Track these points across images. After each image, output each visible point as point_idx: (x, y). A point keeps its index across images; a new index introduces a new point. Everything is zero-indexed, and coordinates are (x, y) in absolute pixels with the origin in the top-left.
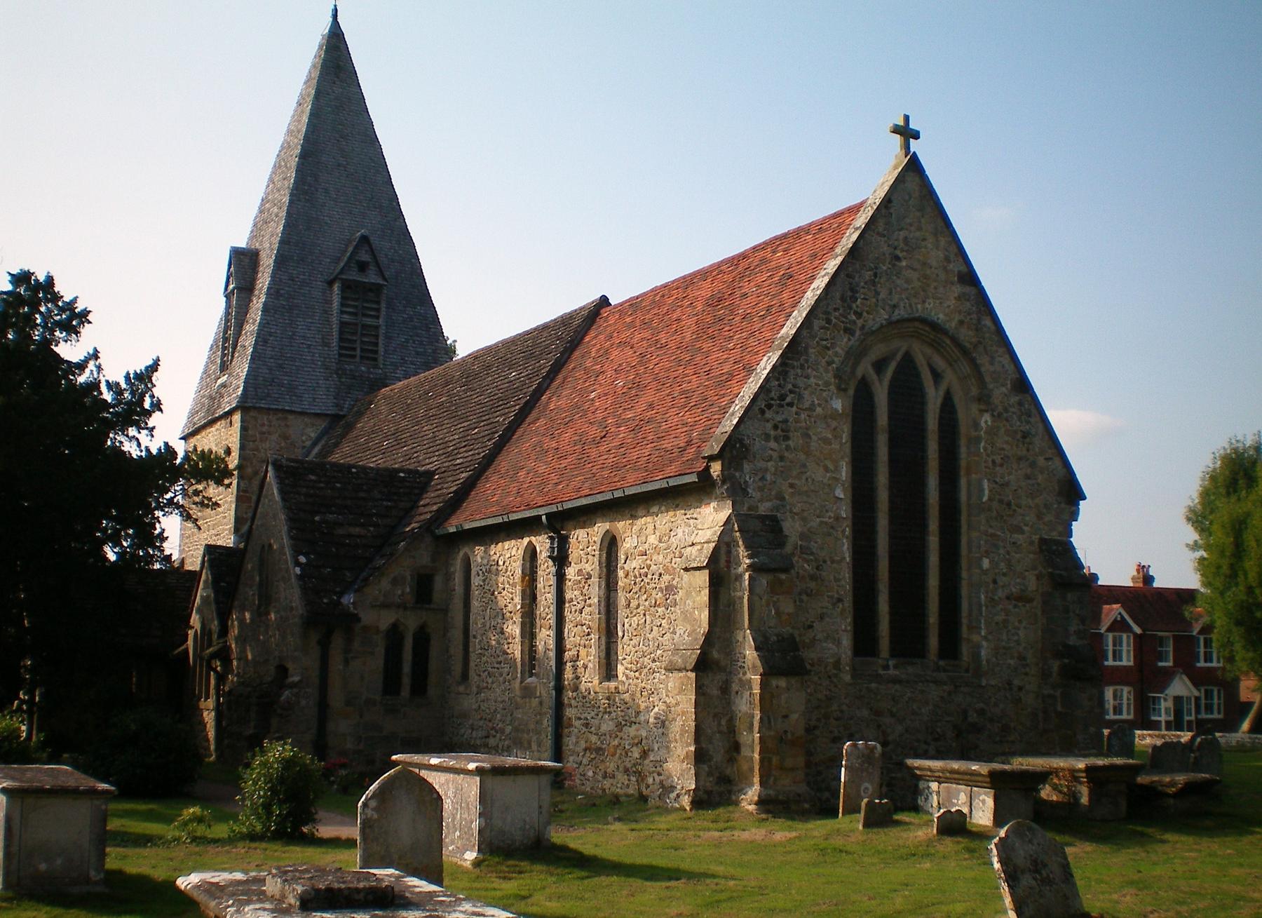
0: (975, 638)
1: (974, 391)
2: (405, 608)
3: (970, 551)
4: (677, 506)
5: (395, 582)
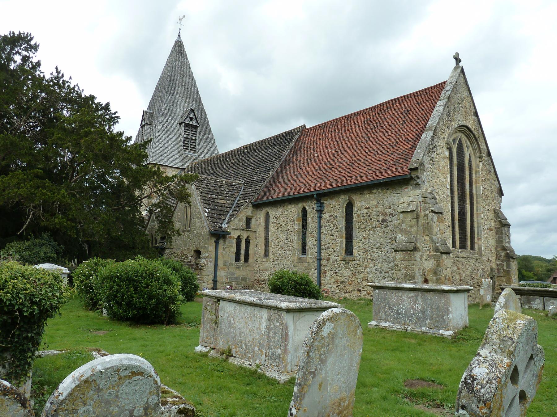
0: (480, 242)
1: (478, 155)
2: (243, 230)
3: (477, 211)
4: (388, 189)
5: (240, 220)
